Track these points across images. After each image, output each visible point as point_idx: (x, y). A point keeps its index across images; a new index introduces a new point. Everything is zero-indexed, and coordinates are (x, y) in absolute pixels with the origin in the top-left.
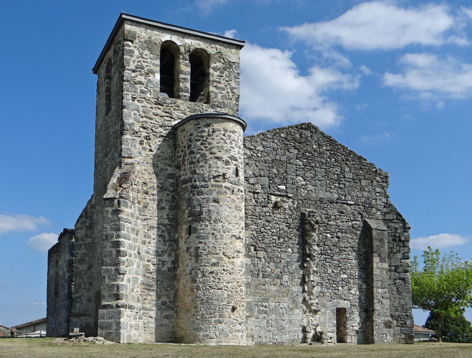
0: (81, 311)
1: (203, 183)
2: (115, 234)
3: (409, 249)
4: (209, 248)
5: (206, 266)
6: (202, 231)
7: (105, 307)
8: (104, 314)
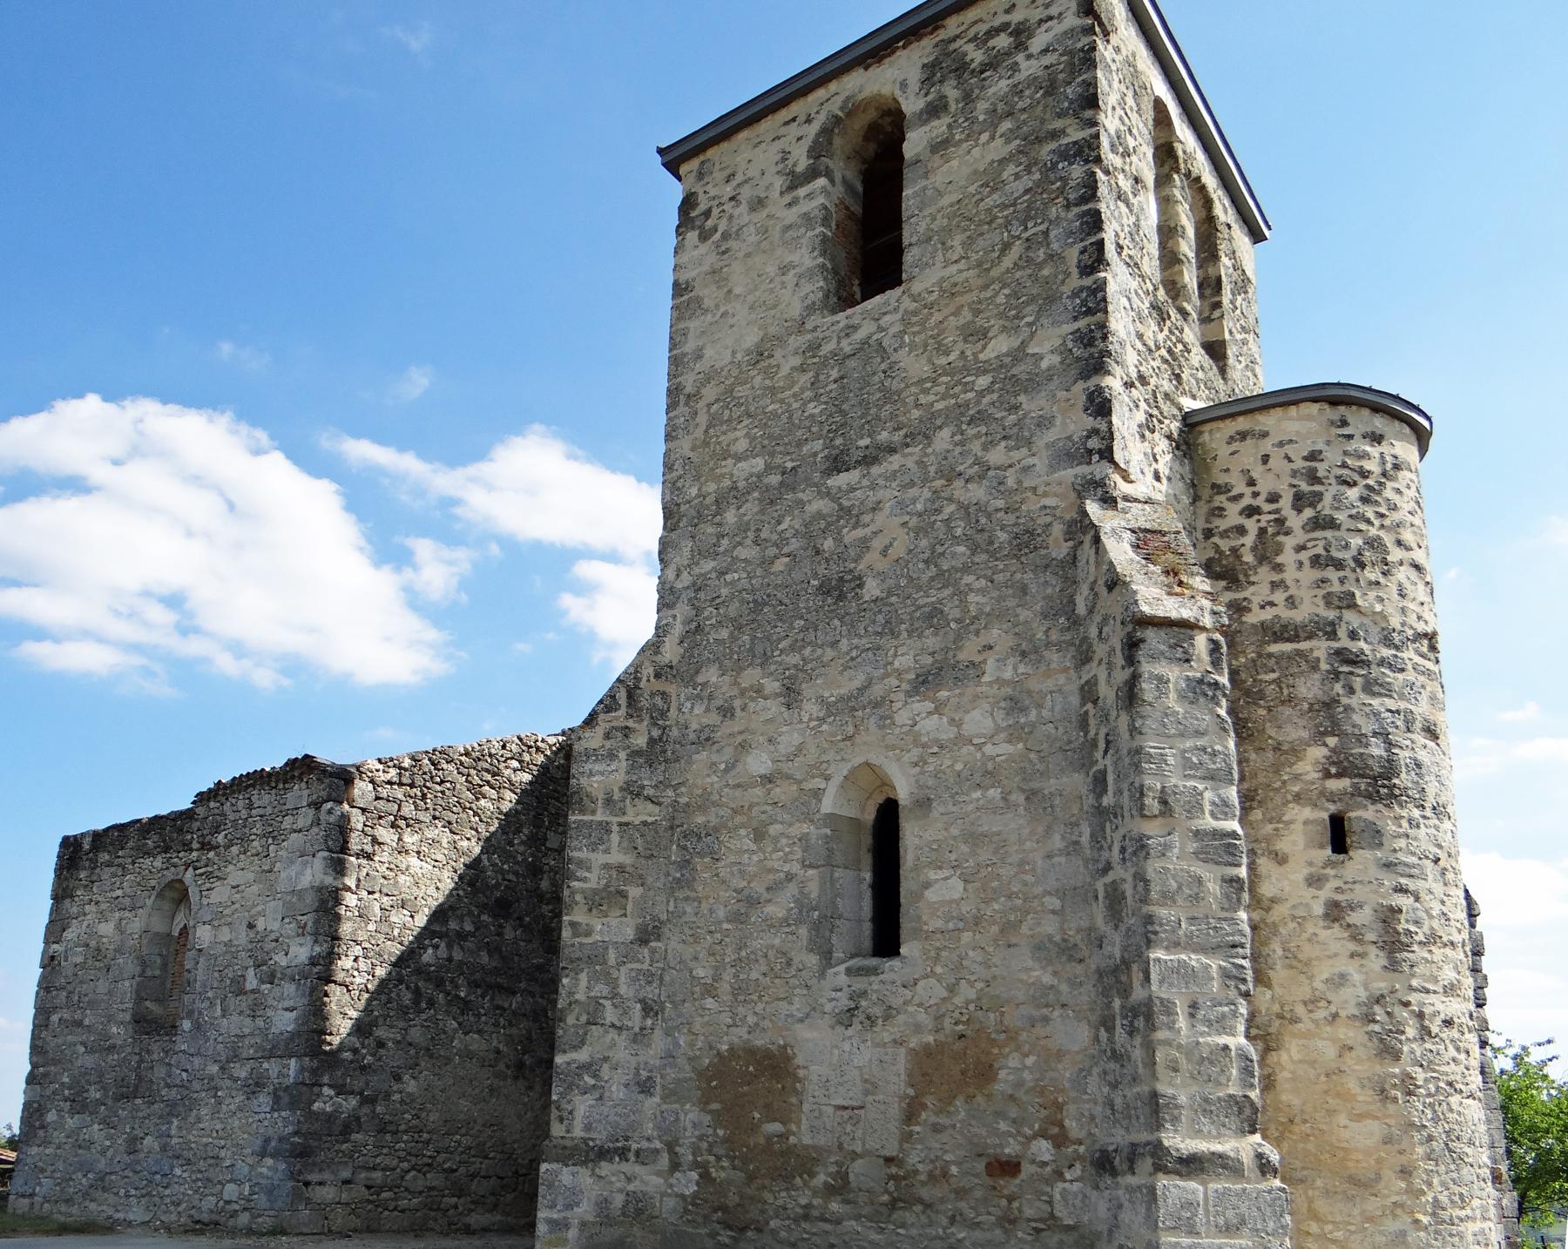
0: (600, 1137)
1: (1387, 652)
2: (1208, 795)
3: (1485, 977)
4: (1431, 917)
5: (1428, 991)
6: (1402, 843)
7: (1192, 1165)
8: (1190, 1205)
